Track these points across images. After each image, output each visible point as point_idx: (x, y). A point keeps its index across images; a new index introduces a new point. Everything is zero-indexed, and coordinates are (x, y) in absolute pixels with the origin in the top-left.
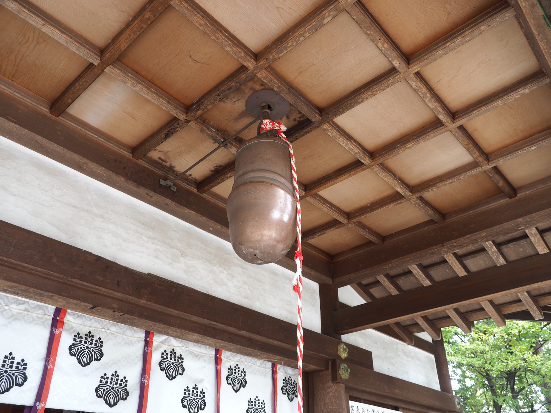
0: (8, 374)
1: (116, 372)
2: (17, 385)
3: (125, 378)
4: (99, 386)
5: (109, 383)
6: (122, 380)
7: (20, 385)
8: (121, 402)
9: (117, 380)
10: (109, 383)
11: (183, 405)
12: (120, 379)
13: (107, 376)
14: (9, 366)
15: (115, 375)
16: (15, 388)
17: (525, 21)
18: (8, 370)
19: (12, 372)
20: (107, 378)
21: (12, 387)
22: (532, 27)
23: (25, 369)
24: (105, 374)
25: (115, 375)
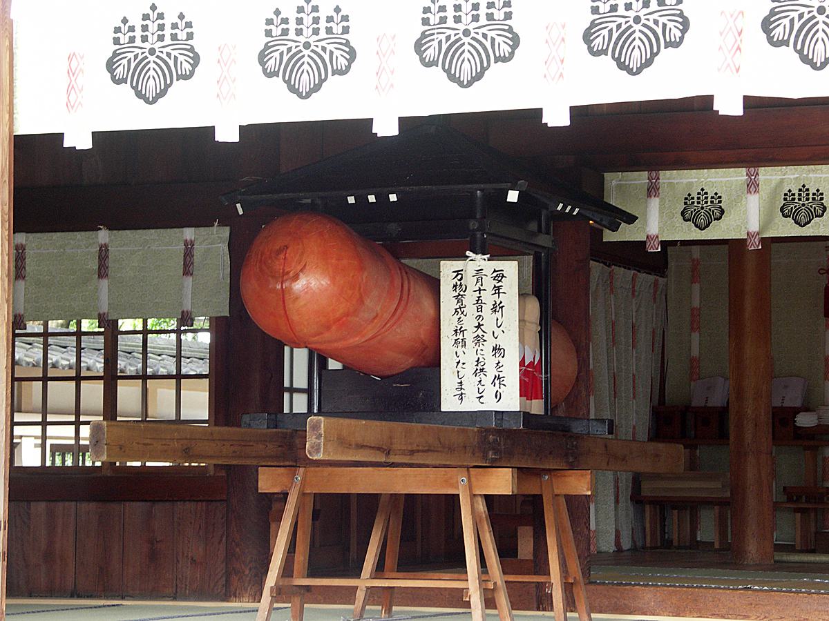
0: (473, 38)
1: (153, 8)
2: (668, 45)
3: (181, 17)
4: (267, 47)
5: (138, 40)
6: (330, 19)
7: (676, 44)
8: (178, 85)
9: (161, 27)
10: (138, 40)
11: (265, 71)
12: (168, 22)
13: (283, 15)
14: (310, 31)
15: (154, 14)
16: (666, 56)
17: (413, 464)
18: (471, 27)
19: (165, 50)
20: (132, 29)
21: (657, 53)
22: (342, 459)
23: (346, 30)
24: (125, 21)
25: (154, 14)
